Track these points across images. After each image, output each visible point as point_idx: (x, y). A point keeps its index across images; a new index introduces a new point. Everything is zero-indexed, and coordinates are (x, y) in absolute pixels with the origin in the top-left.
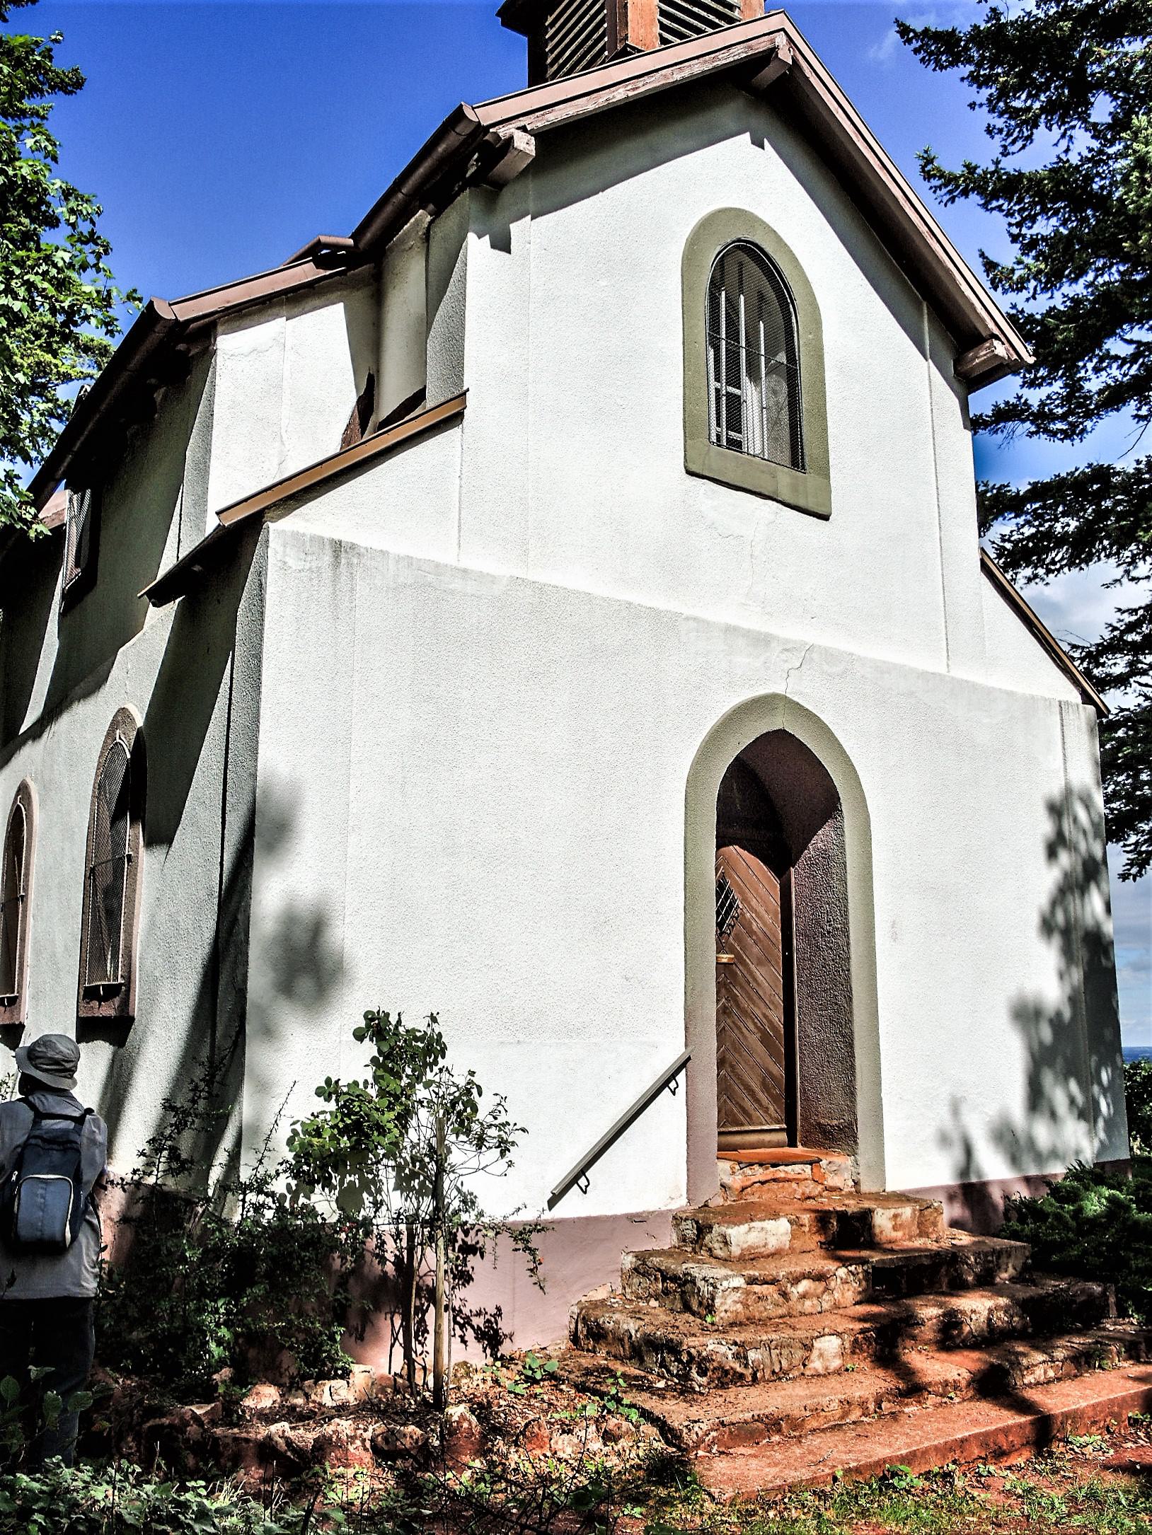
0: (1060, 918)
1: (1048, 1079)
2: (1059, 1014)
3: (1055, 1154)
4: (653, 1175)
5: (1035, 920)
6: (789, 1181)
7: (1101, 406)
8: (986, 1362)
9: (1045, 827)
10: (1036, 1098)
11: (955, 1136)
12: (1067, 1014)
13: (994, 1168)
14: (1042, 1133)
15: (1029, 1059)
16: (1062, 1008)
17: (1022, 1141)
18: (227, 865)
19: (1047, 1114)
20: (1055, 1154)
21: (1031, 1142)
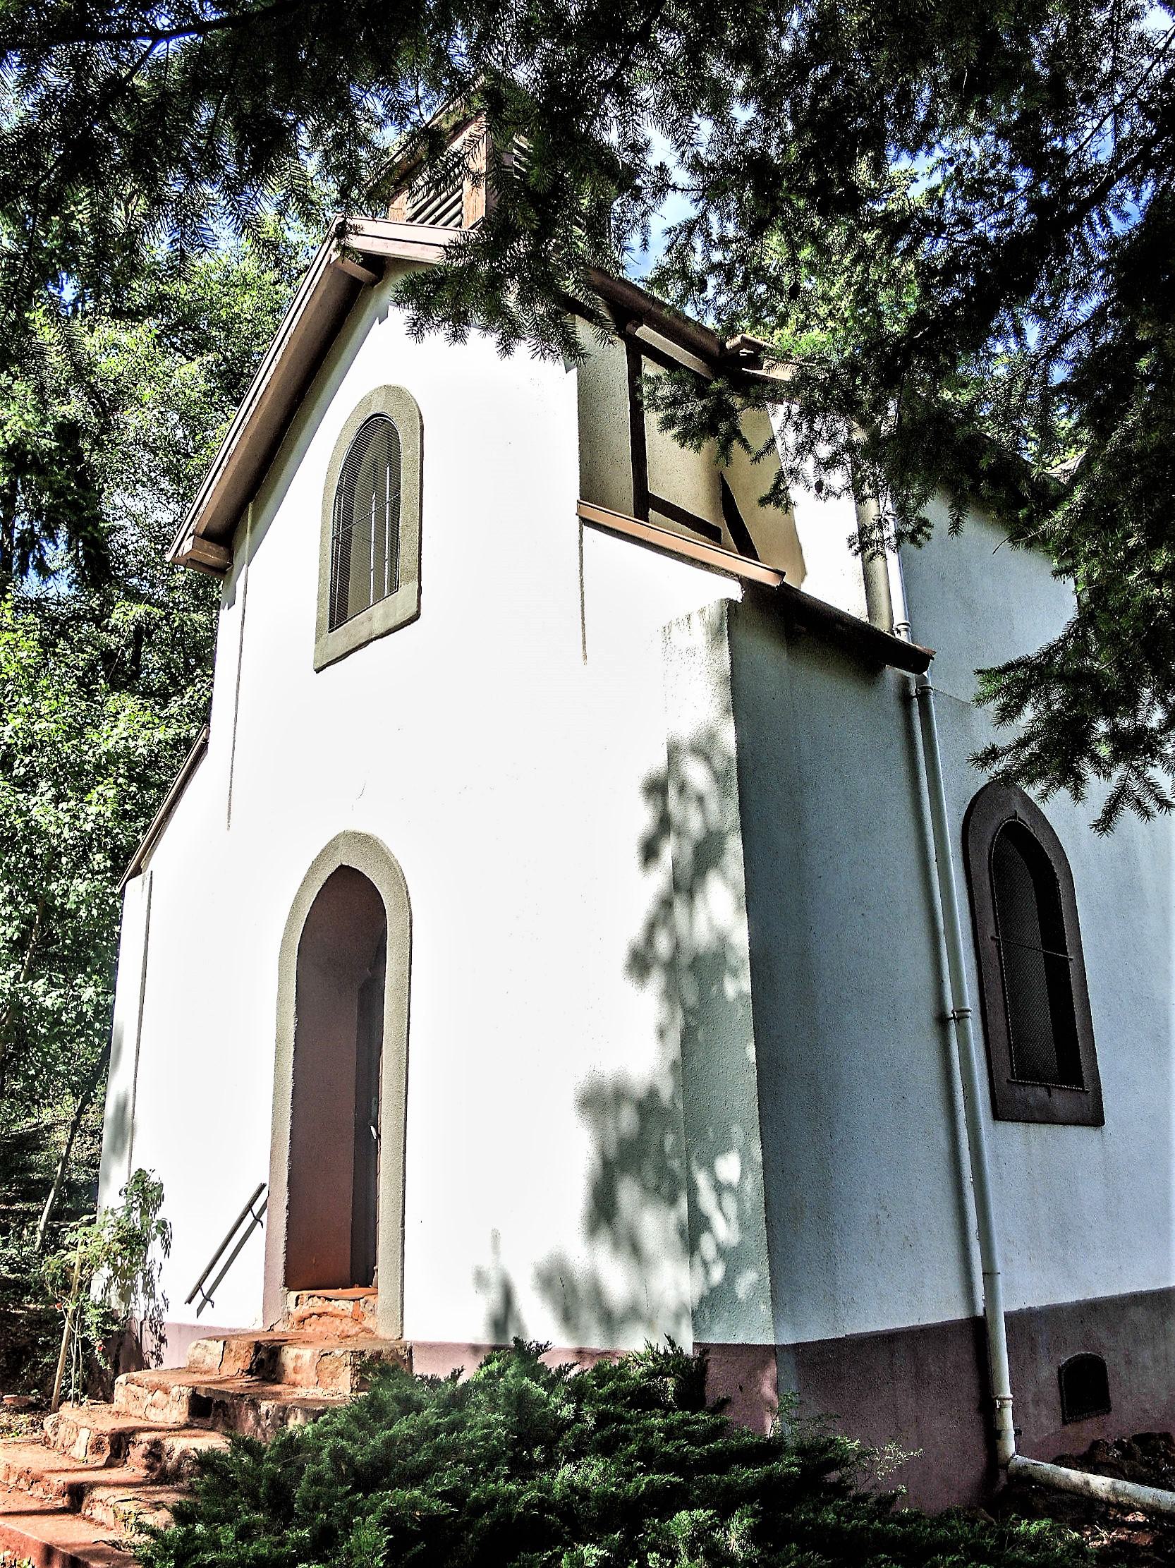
0: (663, 945)
1: (628, 1193)
2: (653, 1093)
3: (635, 1313)
4: (248, 1299)
5: (621, 956)
6: (335, 1316)
7: (661, 1405)
8: (45, 1148)
9: (643, 818)
10: (603, 1210)
11: (494, 1277)
12: (666, 1090)
13: (539, 1323)
14: (617, 1281)
15: (598, 1162)
16: (658, 1083)
17: (583, 1290)
18: (128, 1146)
19: (628, 1249)
20: (635, 1313)
21: (597, 1293)
